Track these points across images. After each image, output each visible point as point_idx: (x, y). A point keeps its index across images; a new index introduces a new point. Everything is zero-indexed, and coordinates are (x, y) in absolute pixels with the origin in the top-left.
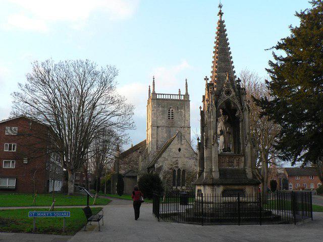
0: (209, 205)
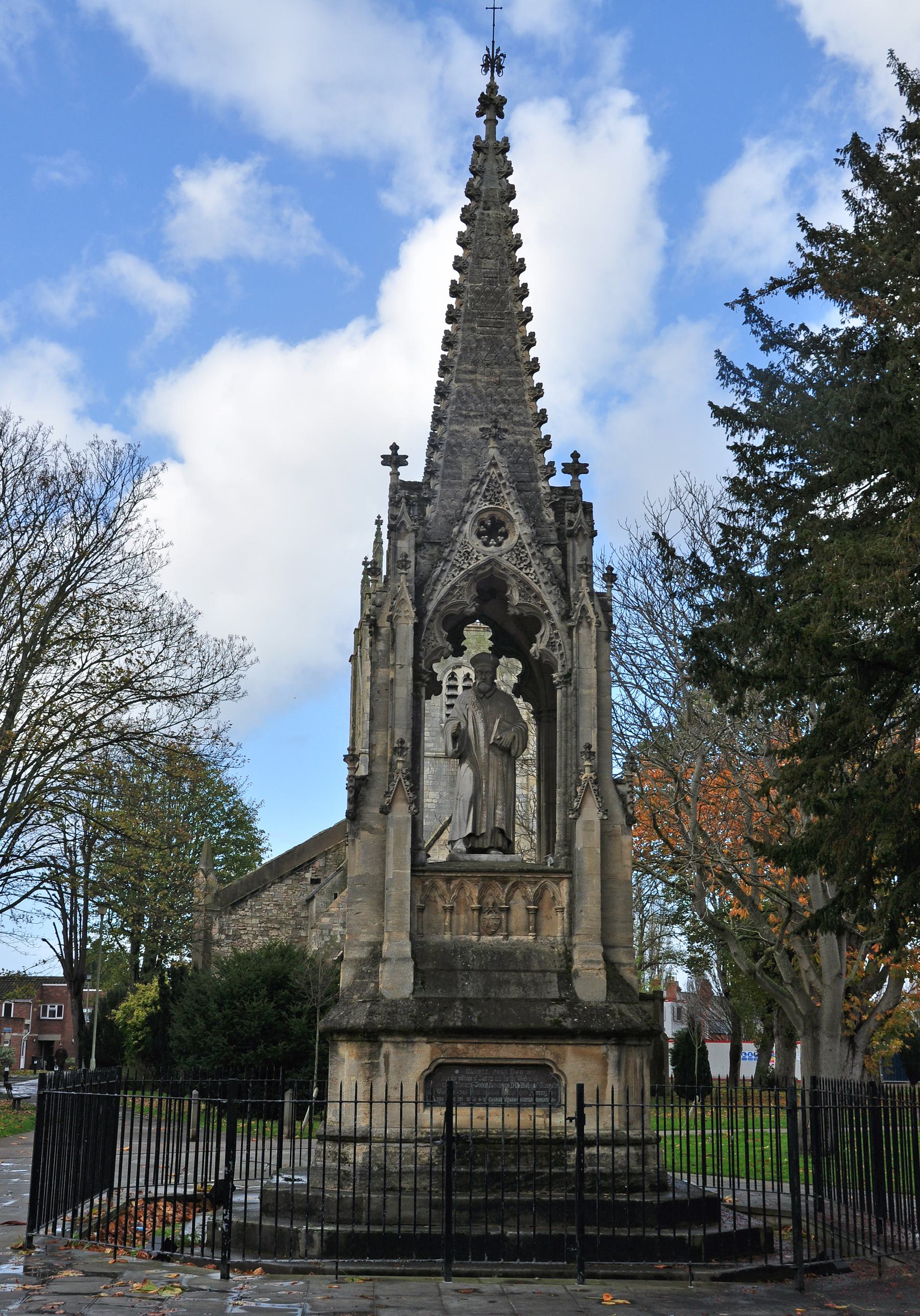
0: (348, 1149)
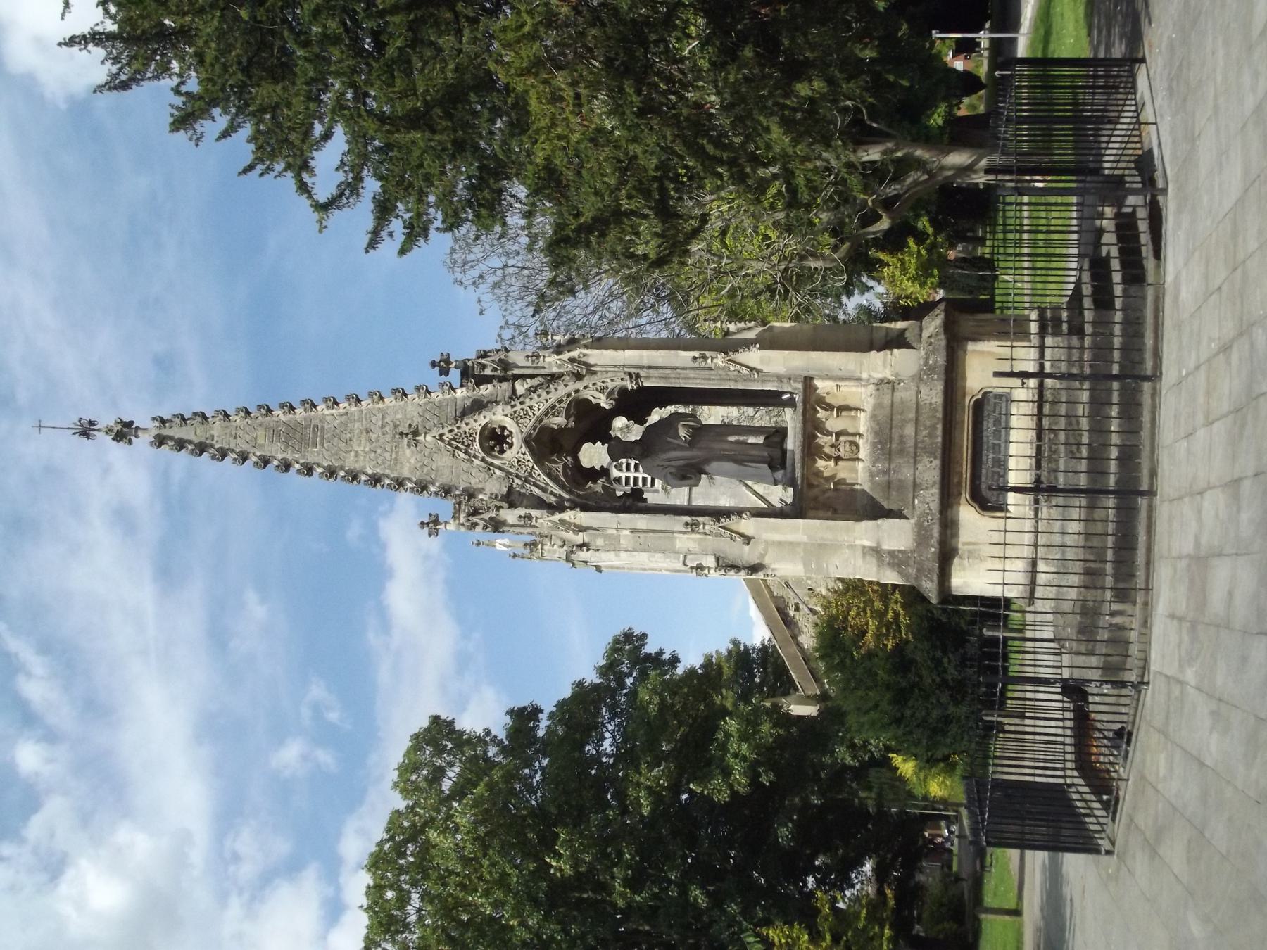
0: (1041, 578)
